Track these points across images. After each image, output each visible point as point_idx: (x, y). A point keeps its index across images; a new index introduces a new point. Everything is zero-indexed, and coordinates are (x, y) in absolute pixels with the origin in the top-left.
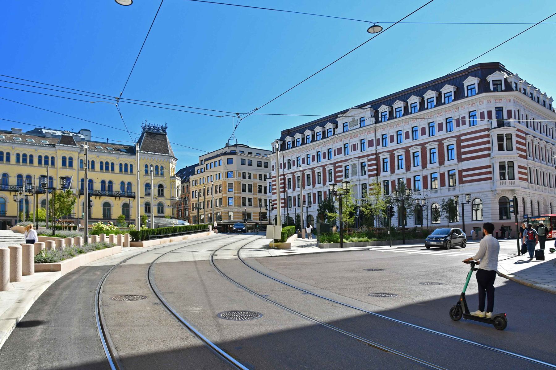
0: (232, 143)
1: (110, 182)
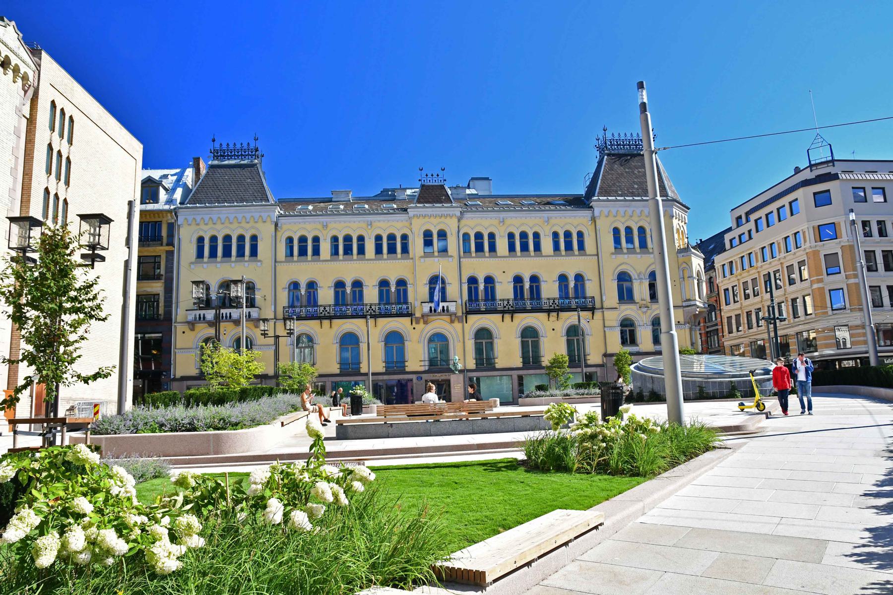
0: (822, 155)
1: (534, 279)
